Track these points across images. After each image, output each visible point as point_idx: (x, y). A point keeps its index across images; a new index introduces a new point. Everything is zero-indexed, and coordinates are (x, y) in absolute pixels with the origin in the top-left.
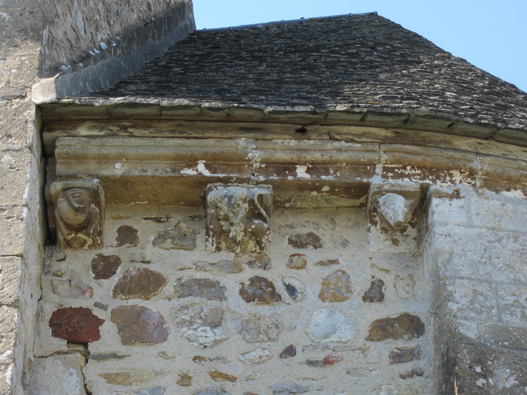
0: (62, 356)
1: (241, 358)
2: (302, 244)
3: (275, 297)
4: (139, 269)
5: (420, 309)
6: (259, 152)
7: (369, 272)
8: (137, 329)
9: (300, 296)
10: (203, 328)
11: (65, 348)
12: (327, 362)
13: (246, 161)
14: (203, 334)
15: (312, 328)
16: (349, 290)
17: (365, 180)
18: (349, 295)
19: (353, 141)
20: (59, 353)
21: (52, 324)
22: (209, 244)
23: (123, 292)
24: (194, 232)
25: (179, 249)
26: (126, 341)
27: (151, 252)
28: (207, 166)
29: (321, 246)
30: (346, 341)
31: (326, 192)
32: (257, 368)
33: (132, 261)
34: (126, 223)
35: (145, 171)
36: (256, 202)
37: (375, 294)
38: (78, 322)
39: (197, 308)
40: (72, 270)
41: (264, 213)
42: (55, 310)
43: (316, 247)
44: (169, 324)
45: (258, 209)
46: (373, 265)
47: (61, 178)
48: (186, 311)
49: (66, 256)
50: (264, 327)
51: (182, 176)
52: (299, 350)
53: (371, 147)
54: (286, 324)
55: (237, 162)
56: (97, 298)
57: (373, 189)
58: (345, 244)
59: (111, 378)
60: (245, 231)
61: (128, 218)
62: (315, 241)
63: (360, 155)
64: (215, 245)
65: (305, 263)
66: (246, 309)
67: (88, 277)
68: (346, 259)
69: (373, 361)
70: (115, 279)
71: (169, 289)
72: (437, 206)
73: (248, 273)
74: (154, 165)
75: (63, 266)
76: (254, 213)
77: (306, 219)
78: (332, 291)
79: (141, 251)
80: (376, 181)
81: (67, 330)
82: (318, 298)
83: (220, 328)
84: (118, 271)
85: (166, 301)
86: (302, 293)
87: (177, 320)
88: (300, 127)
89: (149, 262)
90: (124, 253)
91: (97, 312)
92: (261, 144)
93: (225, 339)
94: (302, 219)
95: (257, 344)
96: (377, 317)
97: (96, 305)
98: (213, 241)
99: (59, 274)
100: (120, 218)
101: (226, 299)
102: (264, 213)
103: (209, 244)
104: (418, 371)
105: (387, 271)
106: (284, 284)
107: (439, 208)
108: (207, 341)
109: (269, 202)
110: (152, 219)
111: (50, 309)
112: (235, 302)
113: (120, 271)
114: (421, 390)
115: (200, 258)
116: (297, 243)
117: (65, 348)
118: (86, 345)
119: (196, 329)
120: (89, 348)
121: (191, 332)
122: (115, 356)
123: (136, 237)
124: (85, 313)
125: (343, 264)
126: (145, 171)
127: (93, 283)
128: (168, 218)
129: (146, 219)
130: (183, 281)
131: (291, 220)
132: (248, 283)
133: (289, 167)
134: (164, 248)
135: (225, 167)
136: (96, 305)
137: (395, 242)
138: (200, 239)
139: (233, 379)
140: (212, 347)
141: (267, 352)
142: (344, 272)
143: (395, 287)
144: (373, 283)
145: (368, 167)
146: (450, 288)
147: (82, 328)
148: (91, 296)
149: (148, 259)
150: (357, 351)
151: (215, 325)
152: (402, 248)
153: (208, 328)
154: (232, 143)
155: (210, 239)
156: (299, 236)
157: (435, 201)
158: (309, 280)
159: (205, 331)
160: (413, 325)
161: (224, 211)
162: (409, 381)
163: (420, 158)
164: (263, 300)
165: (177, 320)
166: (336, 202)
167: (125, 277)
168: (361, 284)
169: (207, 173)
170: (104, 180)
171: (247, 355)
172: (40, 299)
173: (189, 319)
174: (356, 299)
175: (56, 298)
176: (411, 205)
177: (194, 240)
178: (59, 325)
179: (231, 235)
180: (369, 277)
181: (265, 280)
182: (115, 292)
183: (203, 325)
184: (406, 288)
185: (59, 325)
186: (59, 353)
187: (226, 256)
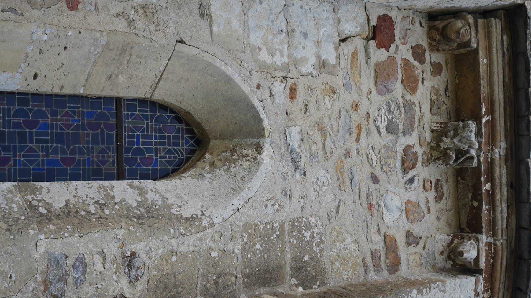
0: (366, 22)
1: (370, 146)
2: (437, 188)
3: (405, 170)
4: (419, 77)
5: (404, 271)
6: (498, 157)
7: (424, 235)
8: (382, 75)
9: (408, 187)
10: (386, 119)
11: (371, 24)
12: (370, 206)
13: (492, 148)
14: (383, 120)
15: (390, 195)
16: (412, 222)
17: (484, 230)
18: (410, 221)
19: (507, 222)
20: (368, 20)
21: (385, 15)
22: (435, 125)
23: (405, 65)
24: (440, 114)
25: (431, 104)
26: (377, 65)
27: (428, 84)
28: (487, 121)
29: (436, 201)
30: (384, 219)
31: (472, 204)
32: (365, 157)
33: (423, 72)
34: (444, 68)
35: (483, 79)
36: (468, 155)
37: (411, 239)
38: (387, 34)
39: (398, 116)
40: (415, 31)
41: (460, 161)
42: (393, 18)
43: (436, 198)
44: (388, 96)
45: (462, 157)
46: (428, 237)
47: (476, 23)
48: (396, 108)
49: (423, 27)
50: (389, 161)
51: (481, 104)
52: (377, 186)
53: (504, 234)
54: (391, 178)
55: (492, 142)
56: (401, 47)
57: (479, 236)
58: (439, 218)
59: (354, 54)
60: (448, 148)
61: (447, 69)
62: (439, 198)
63: (500, 227)
64: (436, 128)
65: (427, 191)
66: (400, 148)
67: (412, 42)
68: (430, 219)
69: (373, 238)
70: (412, 60)
71: (408, 97)
72: (471, 281)
73: (419, 151)
74: (486, 85)
75: (418, 25)
76: (460, 153)
77: (451, 191)
78: (412, 209)
79: (429, 78)
80: (484, 238)
81: (382, 26)
82: (407, 199)
83: (386, 132)
84: (416, 62)
85: (401, 95)
86: (410, 188)
87: (391, 102)
88: (514, 185)
89: (423, 83)
90: (427, 67)
91: (393, 46)
92: (503, 158)
93: (380, 135)
94: (451, 189)
95: (379, 157)
96: (398, 240)
97: (397, 46)
98: (438, 127)
99: (413, 22)
100: (447, 65)
101: (404, 135)
102: (460, 161)
103: (435, 125)
104: (368, 270)
105: (424, 248)
106: (414, 176)
107: (469, 282)
108: (379, 123)
109: (467, 165)
110: (447, 86)
111: (393, 14)
112: (404, 141)
113: (416, 63)
114: (357, 272)
115: (427, 119)
116: (438, 185)
117: (371, 24)
118: (373, 38)
119: (385, 115)
120: (372, 41)
121: (384, 112)
122: (368, 58)
123: (437, 75)
124: (392, 40)
125: (427, 216)
126: (483, 79)
127: (408, 45)
128: (448, 97)
129: (447, 81)
130: (413, 106)
131: (451, 180)
132: (414, 151)
133: (491, 179)
134: (430, 94)
135: (488, 133)
136: (397, 46)
137: (442, 253)
138: (437, 118)
139: (357, 140)
140: (375, 126)
141: (375, 163)
142: (423, 217)
143: (415, 253)
144: (416, 238)
145: (491, 232)
146: (424, 291)
147: (384, 36)
148: (401, 43)
149: (425, 82)
150: (378, 228)
151: (387, 128)
152: (439, 258)
153: (386, 123)
154: (503, 138)
155: (438, 125)
156: (442, 187)
157: (473, 279)
158: (417, 194)
159: (385, 121)
160: (394, 266)
161: (461, 133)
162: (361, 264)
163: (499, 268)
164: (403, 163)
165: (391, 102)
166: (464, 211)
167: (414, 66)
168: (417, 229)
169: (484, 120)
170: (476, 51)
171: (372, 150)
172: (399, 9)
173: (392, 110)
174: (407, 226)
175: (399, 19)
176: (470, 262)
177: (436, 115)
178: (384, 21)
179: (444, 138)
180: (421, 236)
181: (416, 163)
182: (405, 60)
183: (388, 120)
184: (415, 261)
185: (384, 21)
186: (368, 20)
187: (428, 136)
